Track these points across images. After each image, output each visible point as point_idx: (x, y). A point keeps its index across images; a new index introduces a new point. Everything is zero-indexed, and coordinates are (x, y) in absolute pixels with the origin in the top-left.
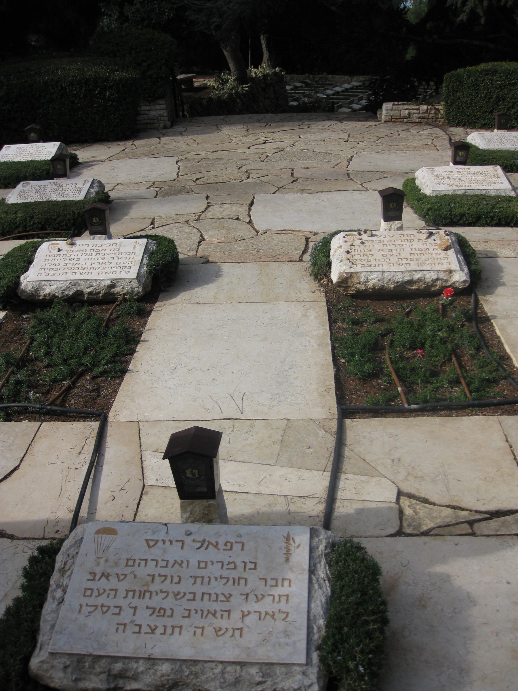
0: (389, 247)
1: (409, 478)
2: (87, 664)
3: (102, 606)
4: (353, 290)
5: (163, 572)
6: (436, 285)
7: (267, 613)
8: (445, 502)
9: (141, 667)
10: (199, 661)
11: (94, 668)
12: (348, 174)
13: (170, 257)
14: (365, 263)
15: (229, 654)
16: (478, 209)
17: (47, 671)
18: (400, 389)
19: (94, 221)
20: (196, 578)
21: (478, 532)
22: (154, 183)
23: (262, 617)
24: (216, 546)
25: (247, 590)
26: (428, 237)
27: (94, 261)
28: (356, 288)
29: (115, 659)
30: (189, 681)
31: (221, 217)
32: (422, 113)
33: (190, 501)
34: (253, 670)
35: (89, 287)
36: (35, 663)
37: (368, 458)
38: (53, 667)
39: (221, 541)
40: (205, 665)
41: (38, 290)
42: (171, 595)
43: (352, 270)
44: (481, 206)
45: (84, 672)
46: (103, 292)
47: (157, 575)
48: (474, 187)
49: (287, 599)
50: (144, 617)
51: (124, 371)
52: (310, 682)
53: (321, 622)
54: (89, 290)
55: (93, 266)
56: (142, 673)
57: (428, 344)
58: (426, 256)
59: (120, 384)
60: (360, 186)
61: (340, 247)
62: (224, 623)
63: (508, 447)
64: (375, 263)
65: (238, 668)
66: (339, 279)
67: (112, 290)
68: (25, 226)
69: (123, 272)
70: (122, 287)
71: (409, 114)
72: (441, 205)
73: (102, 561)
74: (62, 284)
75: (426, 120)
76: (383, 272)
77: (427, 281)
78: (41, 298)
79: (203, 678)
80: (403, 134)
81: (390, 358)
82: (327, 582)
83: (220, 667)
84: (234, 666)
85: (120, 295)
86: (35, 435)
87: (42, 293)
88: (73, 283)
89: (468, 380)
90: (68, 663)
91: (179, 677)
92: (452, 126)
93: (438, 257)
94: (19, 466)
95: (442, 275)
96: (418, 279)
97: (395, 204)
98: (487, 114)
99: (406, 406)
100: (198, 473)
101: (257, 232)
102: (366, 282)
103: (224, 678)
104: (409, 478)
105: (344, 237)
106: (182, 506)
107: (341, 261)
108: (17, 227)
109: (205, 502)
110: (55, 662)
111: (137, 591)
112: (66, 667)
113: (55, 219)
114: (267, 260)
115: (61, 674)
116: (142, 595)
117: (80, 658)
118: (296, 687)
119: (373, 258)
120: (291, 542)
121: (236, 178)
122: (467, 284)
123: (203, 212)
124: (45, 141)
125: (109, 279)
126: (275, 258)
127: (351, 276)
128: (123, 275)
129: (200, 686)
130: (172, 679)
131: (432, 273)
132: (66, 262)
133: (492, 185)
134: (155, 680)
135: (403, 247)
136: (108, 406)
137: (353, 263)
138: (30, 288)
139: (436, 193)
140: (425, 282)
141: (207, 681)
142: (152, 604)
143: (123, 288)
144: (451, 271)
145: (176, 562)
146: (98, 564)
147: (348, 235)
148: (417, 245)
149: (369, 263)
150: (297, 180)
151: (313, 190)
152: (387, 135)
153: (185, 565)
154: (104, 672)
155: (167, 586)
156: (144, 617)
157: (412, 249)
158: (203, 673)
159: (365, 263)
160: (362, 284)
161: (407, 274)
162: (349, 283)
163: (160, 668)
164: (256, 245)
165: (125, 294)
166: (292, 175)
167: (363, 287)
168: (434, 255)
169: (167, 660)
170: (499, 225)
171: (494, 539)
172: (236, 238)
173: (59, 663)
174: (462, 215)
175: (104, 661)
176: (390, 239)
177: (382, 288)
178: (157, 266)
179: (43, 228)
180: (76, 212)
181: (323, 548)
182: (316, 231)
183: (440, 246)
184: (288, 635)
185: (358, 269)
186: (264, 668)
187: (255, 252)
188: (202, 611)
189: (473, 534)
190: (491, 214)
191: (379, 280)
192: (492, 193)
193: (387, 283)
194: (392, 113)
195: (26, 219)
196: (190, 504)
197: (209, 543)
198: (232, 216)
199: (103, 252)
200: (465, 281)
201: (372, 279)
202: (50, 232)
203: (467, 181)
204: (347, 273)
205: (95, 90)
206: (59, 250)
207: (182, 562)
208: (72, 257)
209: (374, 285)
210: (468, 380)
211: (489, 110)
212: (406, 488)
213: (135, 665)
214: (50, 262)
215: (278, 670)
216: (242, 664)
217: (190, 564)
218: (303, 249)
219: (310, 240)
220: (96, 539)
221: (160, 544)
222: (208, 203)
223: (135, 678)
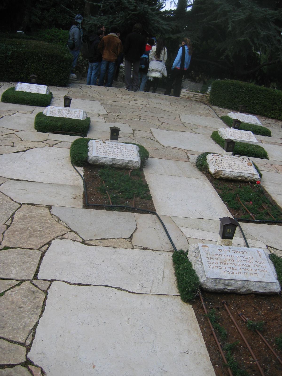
0: (230, 162)
9: (233, 282)
14: (223, 167)
17: (206, 283)
19: (114, 134)
24: (239, 252)
28: (220, 176)
29: (226, 280)
32: (199, 97)
34: (264, 284)
39: (240, 251)
41: (98, 160)
44: (249, 148)
46: (124, 165)
56: (233, 284)
65: (259, 283)
67: (129, 165)
68: (61, 129)
71: (193, 96)
75: (200, 100)
76: (230, 171)
77: (245, 177)
78: (97, 164)
80: (193, 106)
88: (113, 159)
92: (213, 105)
95: (251, 176)
98: (229, 102)
108: (58, 128)
109: (229, 240)
110: (209, 280)
113: (75, 127)
115: (210, 284)
124: (38, 84)
125: (127, 160)
131: (248, 174)
133: (251, 139)
144: (254, 174)
147: (214, 155)
148: (240, 163)
151: (173, 129)
152: (187, 105)
154: (223, 284)
155: (230, 262)
158: (250, 284)
159: (223, 167)
167: (222, 176)
168: (247, 167)
173: (210, 280)
174: (242, 151)
175: (223, 280)
177: (229, 178)
179: (69, 131)
190: (253, 152)
194: (186, 94)
195: (62, 125)
198: (148, 137)
201: (226, 174)
202: (72, 132)
203: (241, 136)
205: (55, 61)
209: (227, 176)
211: (230, 101)
212: (269, 245)
213: (231, 282)
215: (270, 284)
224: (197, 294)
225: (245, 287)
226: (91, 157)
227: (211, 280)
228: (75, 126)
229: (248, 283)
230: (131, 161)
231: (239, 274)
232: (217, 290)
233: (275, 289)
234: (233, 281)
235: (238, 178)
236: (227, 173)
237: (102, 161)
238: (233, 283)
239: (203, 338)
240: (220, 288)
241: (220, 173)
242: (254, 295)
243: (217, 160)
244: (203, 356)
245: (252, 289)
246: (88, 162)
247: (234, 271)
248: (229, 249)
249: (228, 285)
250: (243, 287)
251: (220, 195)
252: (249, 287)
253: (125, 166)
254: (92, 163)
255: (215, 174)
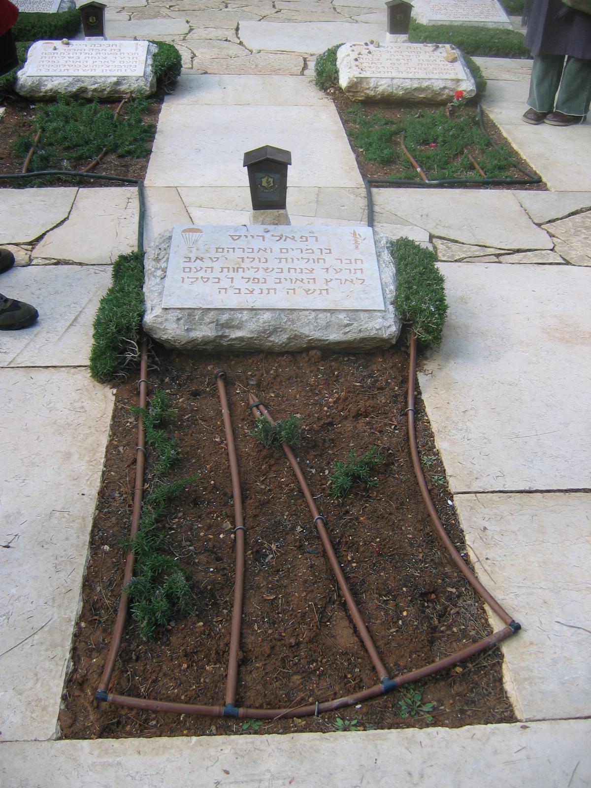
0: (397, 57)
1: (437, 227)
2: (197, 317)
3: (202, 278)
4: (362, 96)
5: (251, 255)
6: (444, 94)
7: (346, 280)
8: (472, 242)
9: (245, 316)
10: (295, 310)
11: (203, 319)
12: (334, 9)
13: (174, 59)
14: (373, 69)
15: (320, 303)
16: (477, 39)
17: (161, 323)
18: (419, 170)
19: (91, 21)
20: (280, 259)
21: (504, 261)
22: (124, 8)
23: (343, 282)
24: (293, 238)
25: (326, 266)
26: (434, 50)
27: (96, 60)
28: (365, 93)
29: (222, 310)
30: (287, 326)
31: (208, 38)
33: (262, 211)
34: (342, 316)
35: (94, 84)
36: (148, 318)
37: (399, 214)
38: (166, 320)
40: (300, 313)
41: (40, 84)
42: (261, 270)
43: (362, 76)
45: (195, 324)
46: (108, 89)
47: (245, 258)
48: (471, 18)
49: (362, 272)
50: (240, 283)
51: (149, 152)
52: (389, 324)
53: (392, 287)
54: (94, 87)
55: (95, 64)
56: (246, 321)
57: (440, 139)
58: (433, 66)
59: (148, 161)
60: (350, 19)
61: (348, 55)
62: (312, 287)
63: (523, 211)
64: (384, 70)
65: (329, 315)
66: (349, 83)
67: (119, 88)
69: (128, 70)
70: (128, 84)
72: (439, 34)
73: (194, 250)
74: (65, 79)
76: (393, 78)
77: (435, 89)
78: (42, 94)
79: (299, 324)
81: (406, 148)
82: (391, 264)
83: (313, 314)
84: (325, 313)
85: (127, 93)
86: (76, 196)
87: (43, 89)
88: (78, 79)
89: (481, 165)
90: (180, 316)
91: (278, 323)
93: (446, 67)
94: (67, 218)
95: (450, 84)
96: (426, 87)
97: (402, 16)
99: (427, 182)
100: (273, 182)
101: (251, 51)
102: (375, 88)
103: (317, 323)
104: (437, 227)
105: (351, 46)
106: (254, 217)
107: (350, 68)
111: (231, 268)
112: (179, 319)
113: (30, 31)
114: (268, 73)
115: (175, 326)
116: (236, 270)
117: (191, 311)
118: (378, 327)
119: (381, 66)
120: (358, 236)
121: (213, 7)
122: (473, 94)
123: (187, 34)
125: (114, 76)
126: (275, 71)
127: (361, 81)
128: (128, 73)
129: (296, 331)
130: (272, 325)
131: (440, 82)
132: (65, 59)
134: (258, 326)
135: (410, 58)
136: (143, 178)
137: (362, 70)
138: (30, 84)
139: (433, 23)
140: (433, 91)
141: (302, 327)
142: (244, 275)
143: (130, 86)
144: (458, 81)
145: (260, 249)
146: (191, 252)
147: (354, 45)
149: (378, 70)
150: (280, 11)
153: (268, 251)
156: (240, 283)
157: (419, 60)
158: (298, 319)
159: (373, 69)
160: (372, 90)
161: (416, 81)
162: (359, 88)
163: (262, 317)
164: (253, 61)
165: (131, 92)
166: (274, 6)
167: (372, 93)
168: (441, 66)
169: (267, 309)
170: (497, 55)
171: (519, 265)
172: (230, 54)
173: (172, 316)
175: (212, 313)
176: (397, 50)
177: (391, 95)
178: (163, 66)
180: (53, 24)
181: (385, 243)
182: (312, 53)
183: (447, 59)
184: (366, 293)
185: (368, 75)
186: (350, 314)
187: (254, 67)
188: (291, 280)
189: (500, 262)
190: (490, 44)
191: (388, 86)
192: (490, 26)
193: (396, 89)
196: (262, 214)
197: (287, 237)
198: (219, 38)
199: (103, 51)
200: (471, 90)
201: (381, 85)
204: (357, 78)
206: (55, 49)
207: (266, 249)
208: (71, 55)
210: (481, 165)
212: (436, 233)
213: (240, 316)
214: (47, 59)
215: (362, 315)
216: (332, 311)
217: (273, 250)
218: (303, 66)
219: (307, 59)
220: (185, 236)
221: (243, 238)
222: (190, 27)
223: (239, 327)
224: (129, 356)
225: (284, 330)
226: (22, 80)
227: (176, 314)
228: (28, 28)
229: (294, 316)
230: (124, 78)
231: (269, 293)
232: (198, 344)
233: (377, 330)
234: (245, 312)
235: (416, 94)
236: (384, 82)
237: (49, 85)
238: (244, 319)
239: (100, 473)
240: (204, 336)
241: (365, 85)
242: (319, 353)
243: (360, 56)
244: (73, 521)
245: (307, 333)
246: (17, 94)
247: (257, 287)
248: (264, 234)
249: (228, 325)
250: (275, 331)
251: (350, 135)
252: (294, 327)
253: (111, 91)
254: (28, 96)
255: (352, 90)
